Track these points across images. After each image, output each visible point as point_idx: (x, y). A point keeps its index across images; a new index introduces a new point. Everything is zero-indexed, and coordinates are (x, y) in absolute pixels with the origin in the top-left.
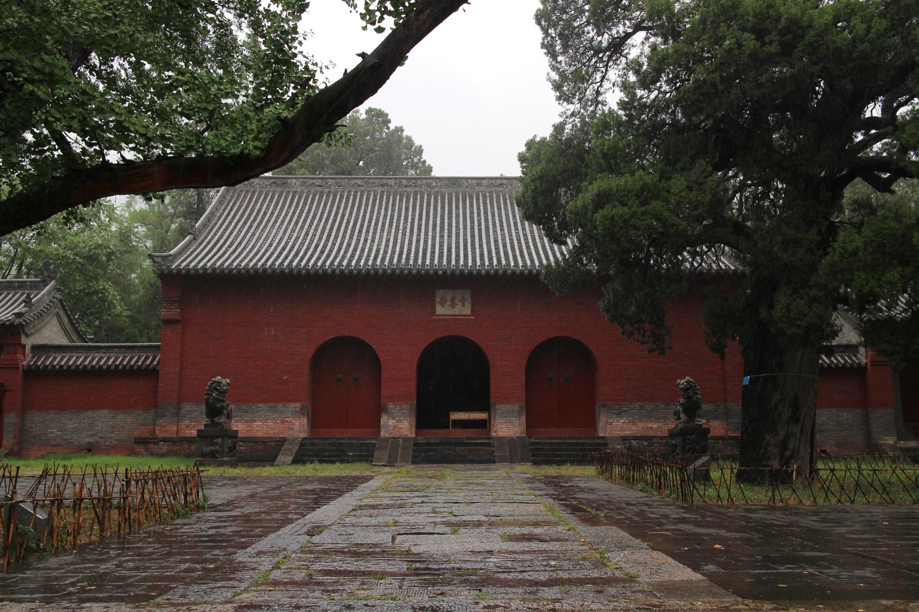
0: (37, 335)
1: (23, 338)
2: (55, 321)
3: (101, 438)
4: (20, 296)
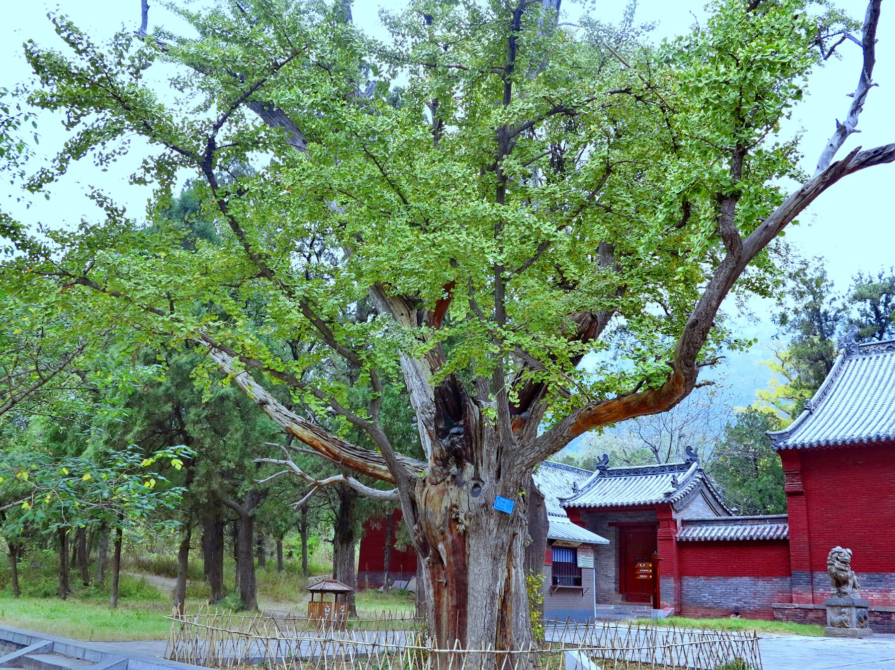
0: (685, 510)
1: (673, 513)
2: (700, 497)
3: (745, 603)
4: (667, 478)
